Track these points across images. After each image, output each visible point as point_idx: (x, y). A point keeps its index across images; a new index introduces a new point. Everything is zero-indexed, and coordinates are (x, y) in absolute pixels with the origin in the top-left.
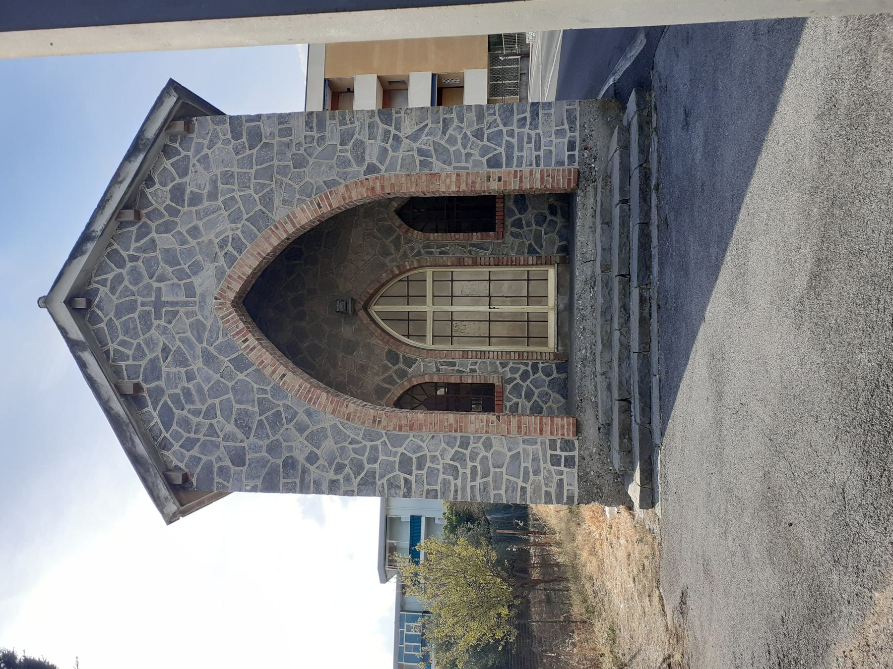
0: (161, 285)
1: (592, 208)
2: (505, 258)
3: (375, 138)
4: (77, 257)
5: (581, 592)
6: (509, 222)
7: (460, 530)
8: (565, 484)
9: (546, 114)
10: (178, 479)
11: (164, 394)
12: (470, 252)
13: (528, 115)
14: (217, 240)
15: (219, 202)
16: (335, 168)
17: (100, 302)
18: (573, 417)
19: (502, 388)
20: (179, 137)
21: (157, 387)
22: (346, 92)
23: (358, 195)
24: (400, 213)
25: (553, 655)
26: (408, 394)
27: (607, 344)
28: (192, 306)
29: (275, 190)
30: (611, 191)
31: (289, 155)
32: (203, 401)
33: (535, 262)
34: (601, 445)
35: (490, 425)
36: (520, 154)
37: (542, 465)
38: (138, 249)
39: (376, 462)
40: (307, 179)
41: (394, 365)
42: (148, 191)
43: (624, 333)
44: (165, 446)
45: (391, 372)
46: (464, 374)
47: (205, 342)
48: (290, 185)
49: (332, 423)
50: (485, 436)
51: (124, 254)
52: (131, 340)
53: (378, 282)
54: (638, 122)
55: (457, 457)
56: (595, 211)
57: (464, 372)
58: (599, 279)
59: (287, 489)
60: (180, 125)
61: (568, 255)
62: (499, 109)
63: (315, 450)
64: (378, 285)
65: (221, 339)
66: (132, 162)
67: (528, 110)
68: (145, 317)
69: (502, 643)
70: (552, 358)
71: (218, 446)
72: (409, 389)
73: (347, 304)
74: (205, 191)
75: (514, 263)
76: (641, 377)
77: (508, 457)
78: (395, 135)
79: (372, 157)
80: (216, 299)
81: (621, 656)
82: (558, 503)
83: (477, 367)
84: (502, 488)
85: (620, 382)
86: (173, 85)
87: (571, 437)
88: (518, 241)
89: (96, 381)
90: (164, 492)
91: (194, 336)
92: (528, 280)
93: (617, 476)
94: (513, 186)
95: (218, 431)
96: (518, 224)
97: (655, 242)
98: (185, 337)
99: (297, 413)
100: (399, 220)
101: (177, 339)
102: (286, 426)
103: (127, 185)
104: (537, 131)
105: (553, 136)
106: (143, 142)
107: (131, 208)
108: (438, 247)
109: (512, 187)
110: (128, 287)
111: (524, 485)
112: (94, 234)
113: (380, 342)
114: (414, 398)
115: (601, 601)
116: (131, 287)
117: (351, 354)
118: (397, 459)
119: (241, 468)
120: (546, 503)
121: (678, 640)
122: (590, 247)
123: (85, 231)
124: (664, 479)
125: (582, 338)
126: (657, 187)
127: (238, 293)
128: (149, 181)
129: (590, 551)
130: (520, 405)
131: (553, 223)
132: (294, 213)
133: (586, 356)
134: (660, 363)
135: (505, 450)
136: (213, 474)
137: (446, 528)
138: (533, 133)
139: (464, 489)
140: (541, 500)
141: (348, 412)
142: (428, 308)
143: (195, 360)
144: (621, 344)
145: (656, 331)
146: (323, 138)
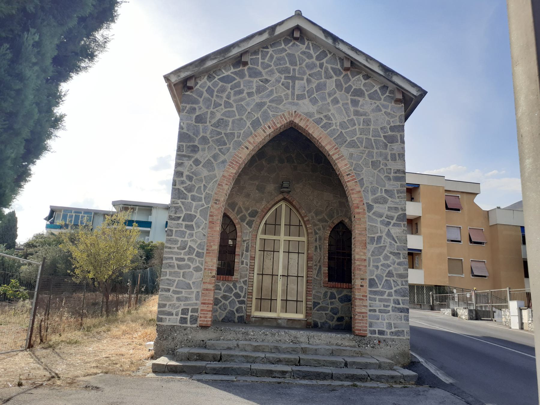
0: (305, 81)
1: (342, 344)
2: (311, 287)
3: (389, 210)
4: (324, 34)
5: (100, 324)
6: (334, 291)
7: (142, 252)
8: (170, 317)
9: (401, 317)
10: (190, 84)
11: (241, 78)
12: (316, 265)
13: (401, 306)
14: (330, 114)
15: (352, 117)
16: (371, 186)
17: (297, 45)
18: (211, 324)
19: (231, 281)
20: (392, 95)
21: (245, 75)
22: (411, 197)
23: (354, 198)
24: (342, 223)
25: (63, 304)
26: (230, 222)
27: (256, 349)
28: (291, 98)
29: (359, 149)
30: (352, 356)
31: (380, 159)
32: (235, 101)
33: (308, 306)
34: (192, 341)
35: (210, 271)
37: (182, 303)
38: (327, 69)
39: (192, 200)
40: (365, 169)
41: (249, 214)
42: (361, 76)
43: (263, 360)
44: (210, 78)
45: (244, 212)
46: (240, 257)
47: (270, 104)
48: (361, 158)
49: (217, 175)
50: (203, 268)
51: (324, 61)
52: (273, 62)
54: (396, 376)
55: (191, 249)
56: (340, 346)
57: (242, 257)
58: (297, 346)
59: (179, 147)
60: (399, 96)
61: (312, 327)
62: (405, 288)
63: (202, 164)
64: (298, 207)
65: (271, 113)
66: (378, 68)
67: (405, 306)
68: (287, 70)
69: (72, 273)
70: (248, 314)
71: (208, 108)
72: (233, 223)
73: (287, 188)
74: (359, 109)
75: (308, 293)
76: (235, 369)
77: (189, 282)
78: (390, 222)
79: (377, 208)
80: (295, 112)
81: (59, 347)
82: (159, 312)
83: (244, 265)
84: (170, 277)
85: (232, 356)
86: (424, 93)
87: (199, 322)
88: (322, 296)
89: (251, 40)
90: (183, 75)
91: (274, 98)
92: (297, 301)
93: (173, 350)
94: (358, 294)
95: (217, 108)
96: (332, 296)
97: (321, 382)
98: (273, 93)
99: (224, 155)
100: (337, 223)
101: (272, 88)
102: (217, 148)
103: (365, 64)
104: (391, 311)
105: (387, 321)
106: (390, 74)
107: (351, 65)
108: (319, 246)
109: (357, 294)
110: (304, 61)
111: (171, 291)
112: (337, 43)
113: (263, 207)
114: (228, 226)
115: (94, 336)
117: (257, 189)
118: (192, 213)
119: (194, 121)
120: (159, 304)
121: (69, 383)
122: (318, 341)
123: (339, 38)
124: (171, 380)
125: (261, 333)
126: (355, 385)
127: (298, 124)
128: (367, 77)
129: (126, 331)
130: (219, 291)
131: (332, 319)
132: (344, 159)
133: (249, 335)
134: (244, 382)
135: (193, 280)
136: (192, 104)
137: (143, 243)
139: (172, 253)
140: (161, 301)
141: (224, 185)
142: (282, 237)
143: (259, 97)
144: (256, 358)
145: (264, 380)
146: (389, 179)
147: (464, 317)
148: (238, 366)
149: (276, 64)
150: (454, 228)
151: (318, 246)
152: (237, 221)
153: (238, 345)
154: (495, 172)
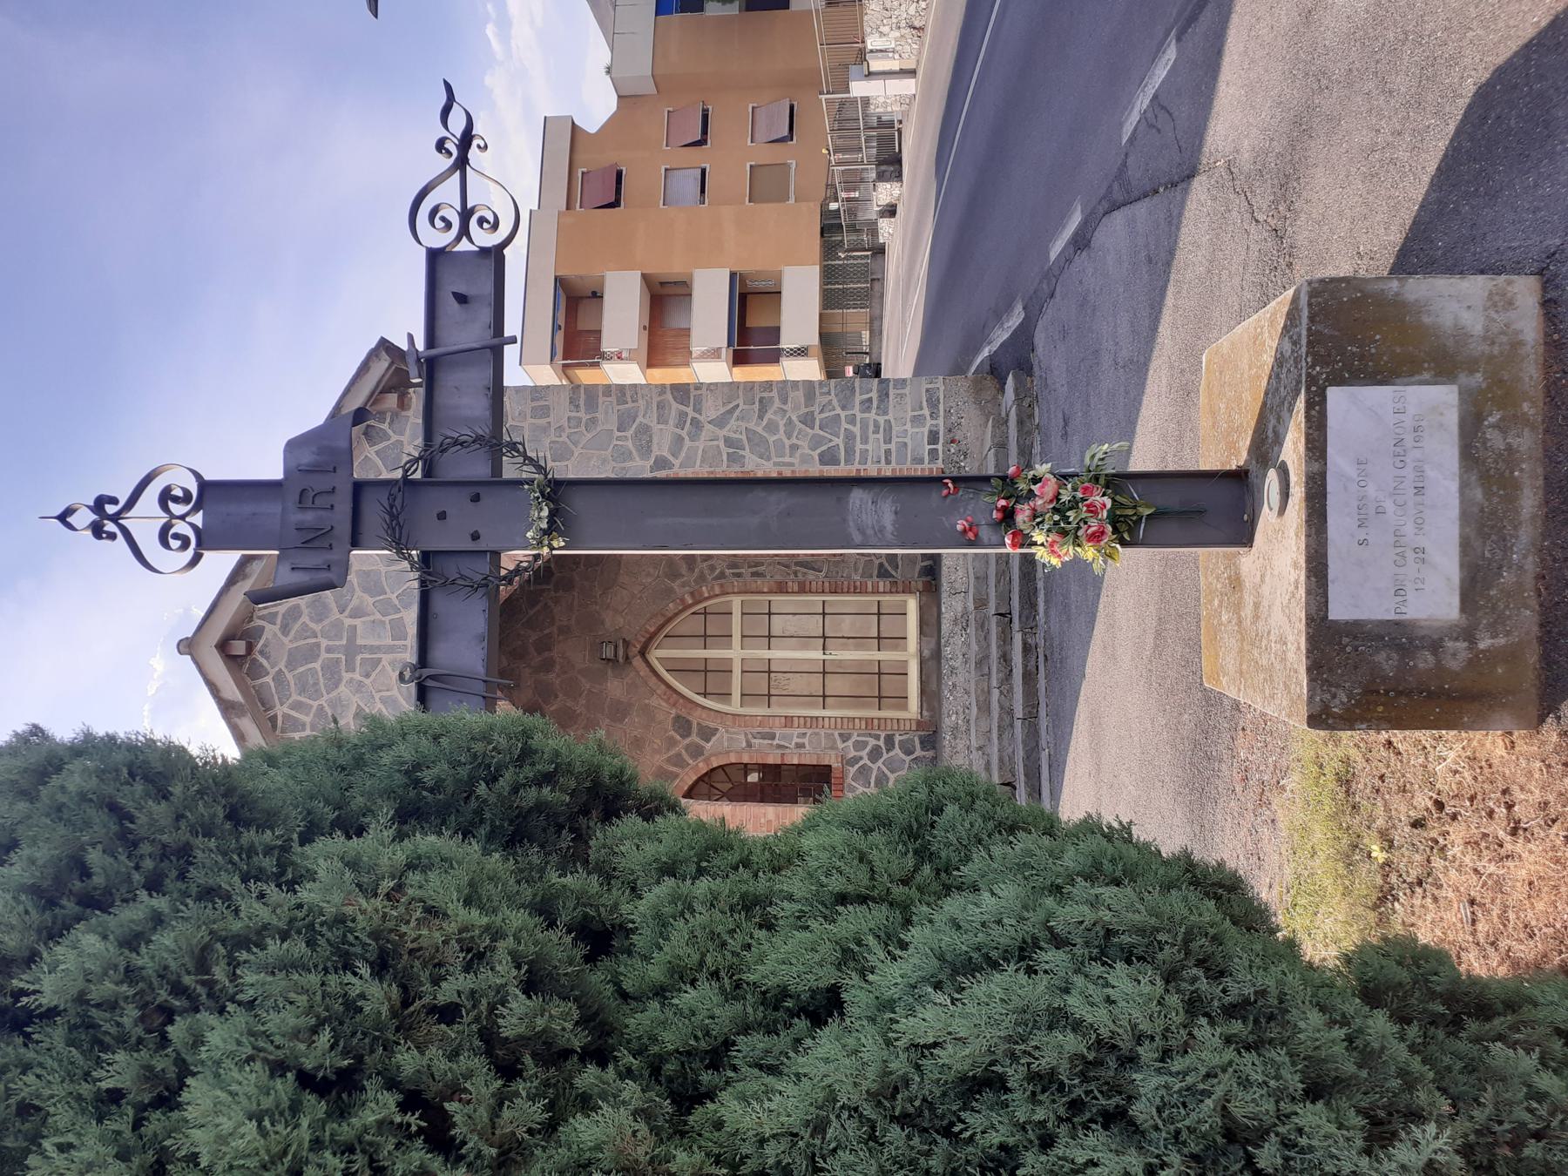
0: (357, 622)
3: (666, 422)
12: (796, 573)
13: (874, 395)
17: (265, 645)
20: (388, 415)
27: (984, 707)
33: (888, 589)
36: (863, 447)
41: (683, 737)
46: (788, 751)
52: (311, 702)
53: (663, 615)
58: (972, 617)
64: (661, 620)
70: (914, 728)
73: (616, 647)
78: (693, 419)
83: (806, 741)
85: (1001, 760)
92: (879, 614)
101: (377, 700)
105: (909, 425)
113: (664, 704)
116: (312, 625)
122: (960, 573)
138: (881, 420)
142: (735, 653)
144: (1001, 707)
146: (593, 421)
147: (896, 192)
148: (1021, 747)
149: (317, 694)
150: (668, 186)
151: (751, 570)
152: (701, 765)
153: (980, 748)
154: (490, 31)
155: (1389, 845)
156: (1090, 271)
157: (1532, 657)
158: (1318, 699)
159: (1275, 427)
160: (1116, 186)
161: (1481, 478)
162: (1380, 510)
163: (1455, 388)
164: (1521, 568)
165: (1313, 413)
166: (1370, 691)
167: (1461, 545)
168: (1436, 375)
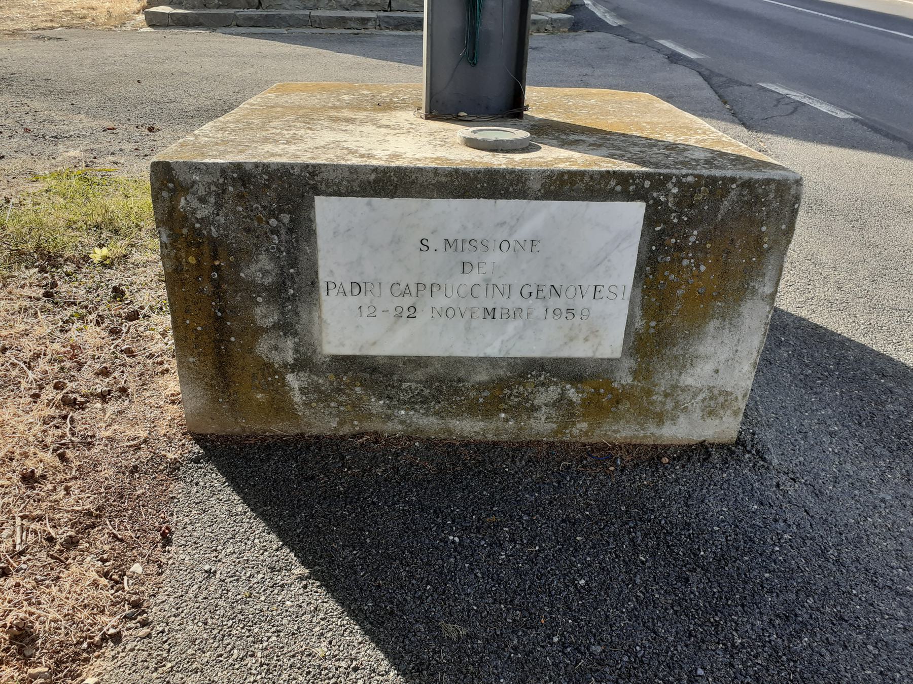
155: (107, 264)
156: (653, 63)
157: (279, 427)
158: (196, 177)
159: (584, 141)
160: (722, 79)
161: (501, 380)
162: (468, 268)
163: (618, 354)
164: (389, 418)
165: (613, 183)
166: (216, 246)
167: (418, 358)
168: (637, 334)
